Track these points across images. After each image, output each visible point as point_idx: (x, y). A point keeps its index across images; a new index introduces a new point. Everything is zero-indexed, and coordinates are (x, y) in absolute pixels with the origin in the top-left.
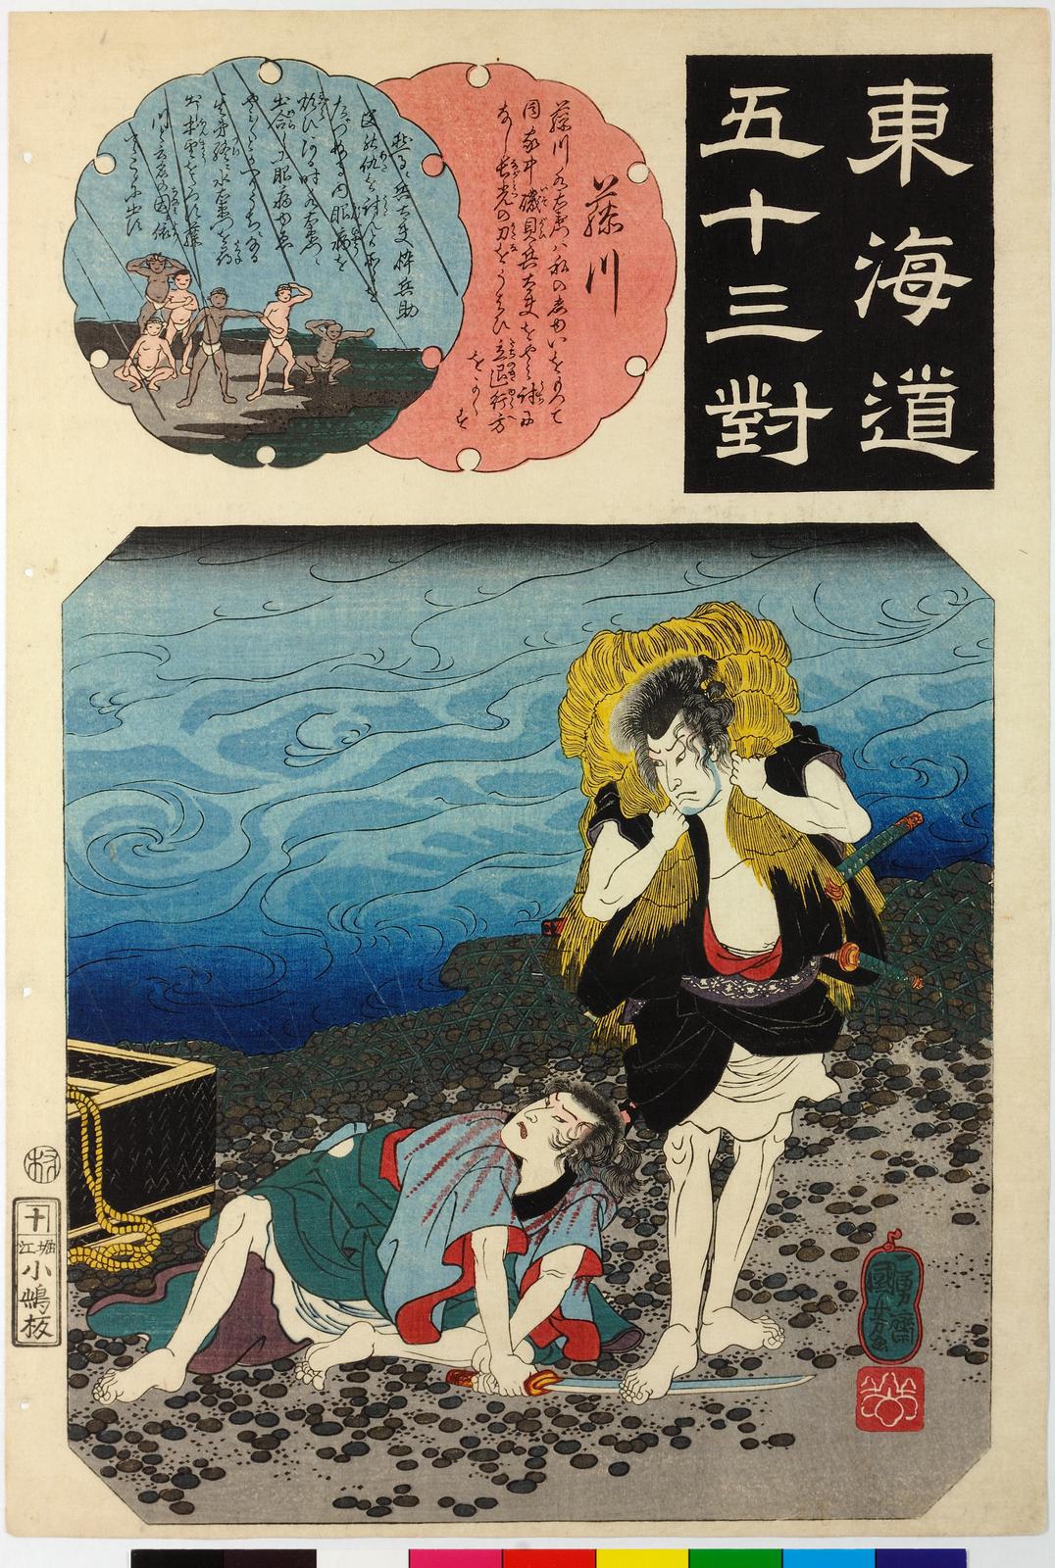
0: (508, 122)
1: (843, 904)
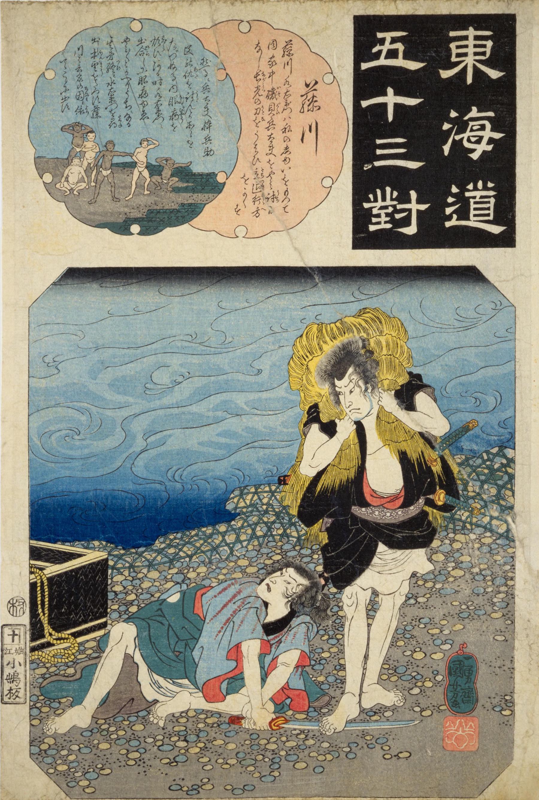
0: (260, 52)
1: (437, 468)
